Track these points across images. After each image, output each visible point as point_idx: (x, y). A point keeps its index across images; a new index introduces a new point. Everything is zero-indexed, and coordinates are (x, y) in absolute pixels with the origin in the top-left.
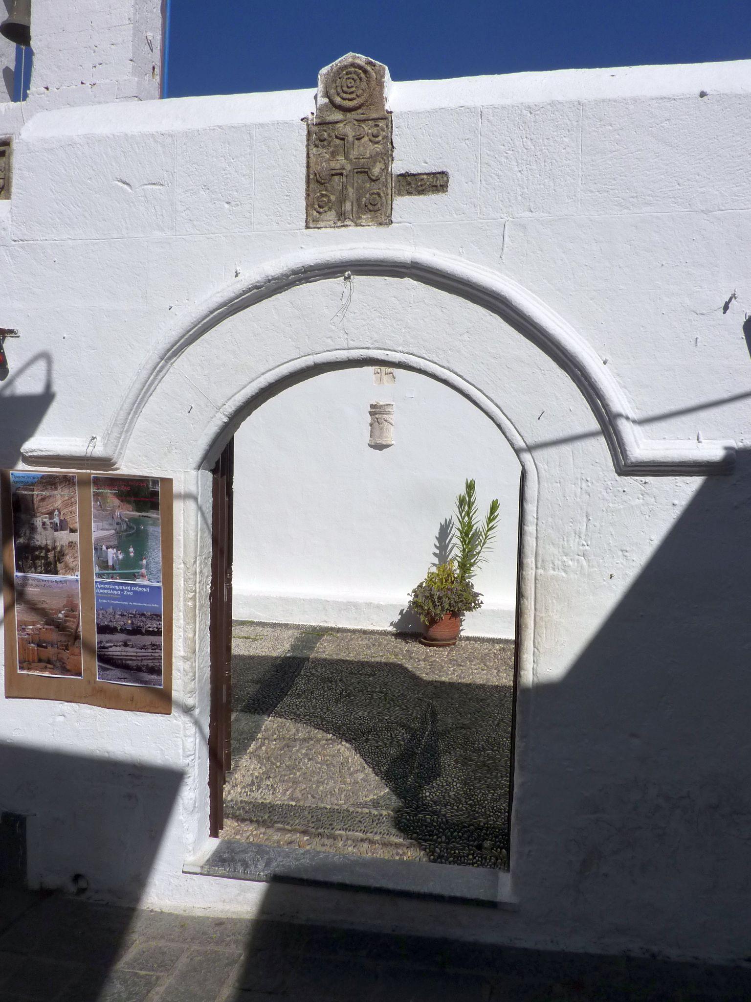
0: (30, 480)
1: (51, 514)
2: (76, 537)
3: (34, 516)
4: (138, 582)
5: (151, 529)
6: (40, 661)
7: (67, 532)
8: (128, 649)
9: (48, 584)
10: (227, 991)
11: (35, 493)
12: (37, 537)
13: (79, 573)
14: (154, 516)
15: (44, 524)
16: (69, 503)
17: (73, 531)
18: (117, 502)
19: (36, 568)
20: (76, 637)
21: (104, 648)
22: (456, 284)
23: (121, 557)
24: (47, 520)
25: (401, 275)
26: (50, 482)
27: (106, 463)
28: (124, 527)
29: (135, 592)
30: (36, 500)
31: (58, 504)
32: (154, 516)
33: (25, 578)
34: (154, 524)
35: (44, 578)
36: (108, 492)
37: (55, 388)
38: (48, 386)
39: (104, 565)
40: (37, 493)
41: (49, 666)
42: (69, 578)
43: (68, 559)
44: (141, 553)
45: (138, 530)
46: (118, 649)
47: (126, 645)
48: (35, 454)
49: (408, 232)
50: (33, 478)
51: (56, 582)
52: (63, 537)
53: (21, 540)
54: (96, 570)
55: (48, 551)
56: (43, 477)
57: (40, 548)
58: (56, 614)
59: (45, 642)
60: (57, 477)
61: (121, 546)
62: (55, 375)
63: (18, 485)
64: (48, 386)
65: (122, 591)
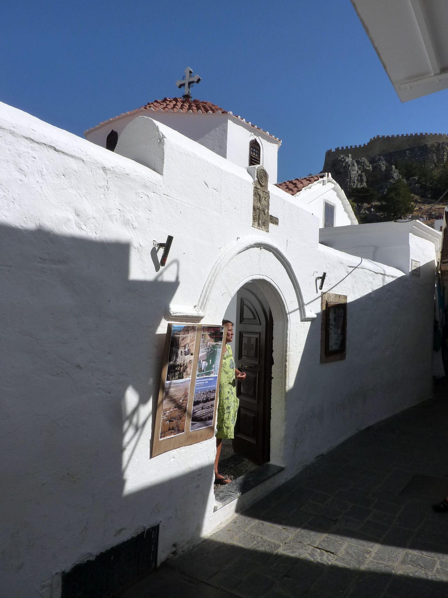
0: (179, 329)
1: (185, 346)
2: (192, 358)
3: (178, 348)
4: (211, 376)
5: (218, 350)
6: (169, 430)
7: (189, 355)
8: (203, 410)
9: (178, 385)
10: (58, 593)
11: (181, 336)
12: (178, 360)
13: (191, 376)
14: (220, 343)
15: (182, 352)
16: (192, 341)
17: (192, 354)
18: (209, 338)
19: (175, 377)
20: (185, 410)
21: (195, 413)
22: (282, 259)
23: (207, 365)
24: (183, 350)
25: (270, 251)
26: (187, 330)
27: (198, 319)
28: (210, 350)
29: (209, 381)
30: (180, 339)
31: (188, 341)
32: (220, 343)
33: (170, 384)
34: (220, 348)
35: (177, 382)
36: (207, 333)
37: (180, 280)
38: (177, 278)
39: (200, 370)
40: (181, 336)
41: (173, 431)
42: (187, 379)
43: (188, 369)
44: (213, 363)
45: (214, 350)
46: (200, 412)
47: (203, 409)
48: (177, 315)
49: (271, 236)
50: (181, 328)
51: (182, 383)
52: (189, 358)
53: (171, 363)
54: (197, 373)
55: (181, 366)
56: (185, 327)
57: (178, 365)
58: (179, 401)
59: (173, 418)
60: (190, 327)
61: (207, 360)
62: (180, 273)
63: (175, 332)
64: (177, 278)
65: (205, 381)
